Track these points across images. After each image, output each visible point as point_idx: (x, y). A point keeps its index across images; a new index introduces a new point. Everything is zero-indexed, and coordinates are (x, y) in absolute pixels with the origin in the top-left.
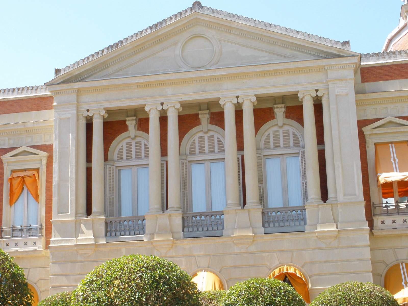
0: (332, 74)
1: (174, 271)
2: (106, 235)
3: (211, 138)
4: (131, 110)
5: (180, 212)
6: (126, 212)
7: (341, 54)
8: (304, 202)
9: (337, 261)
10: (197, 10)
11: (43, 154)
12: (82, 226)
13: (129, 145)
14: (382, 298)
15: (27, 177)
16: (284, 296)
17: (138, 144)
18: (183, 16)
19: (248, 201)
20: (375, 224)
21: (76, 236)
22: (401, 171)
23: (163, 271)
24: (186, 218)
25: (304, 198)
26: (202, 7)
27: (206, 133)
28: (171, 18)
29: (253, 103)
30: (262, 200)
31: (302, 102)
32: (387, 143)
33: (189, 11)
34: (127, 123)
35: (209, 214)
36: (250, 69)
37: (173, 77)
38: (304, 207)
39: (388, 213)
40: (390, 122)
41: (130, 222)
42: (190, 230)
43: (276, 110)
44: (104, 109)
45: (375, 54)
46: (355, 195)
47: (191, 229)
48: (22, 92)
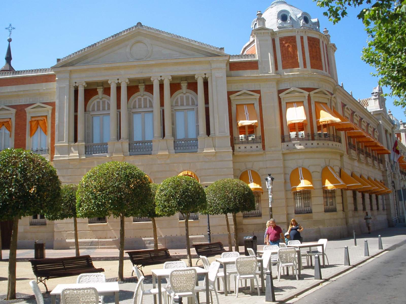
0: (214, 65)
1: (137, 170)
2: (85, 154)
3: (145, 99)
4: (100, 83)
5: (128, 140)
6: (96, 140)
7: (219, 54)
8: (197, 136)
9: (215, 169)
10: (139, 27)
11: (50, 108)
12: (72, 148)
13: (98, 102)
14: (244, 187)
15: (41, 121)
16: (193, 185)
17: (104, 102)
18: (131, 30)
19: (166, 135)
20: (235, 148)
21: (69, 154)
22: (250, 120)
23: (131, 171)
24: (131, 144)
25: (197, 134)
26: (142, 26)
27: (142, 96)
28: (124, 31)
29: (170, 80)
30: (174, 134)
31: (197, 80)
32: (243, 105)
33: (134, 27)
34: (98, 90)
35: (143, 142)
36: (169, 61)
37: (125, 64)
38: (197, 138)
39: (242, 143)
40: (245, 93)
41: (99, 146)
42: (133, 151)
43: (182, 84)
44: (85, 82)
45: (237, 55)
46: (225, 132)
47: (133, 151)
48: (37, 72)
